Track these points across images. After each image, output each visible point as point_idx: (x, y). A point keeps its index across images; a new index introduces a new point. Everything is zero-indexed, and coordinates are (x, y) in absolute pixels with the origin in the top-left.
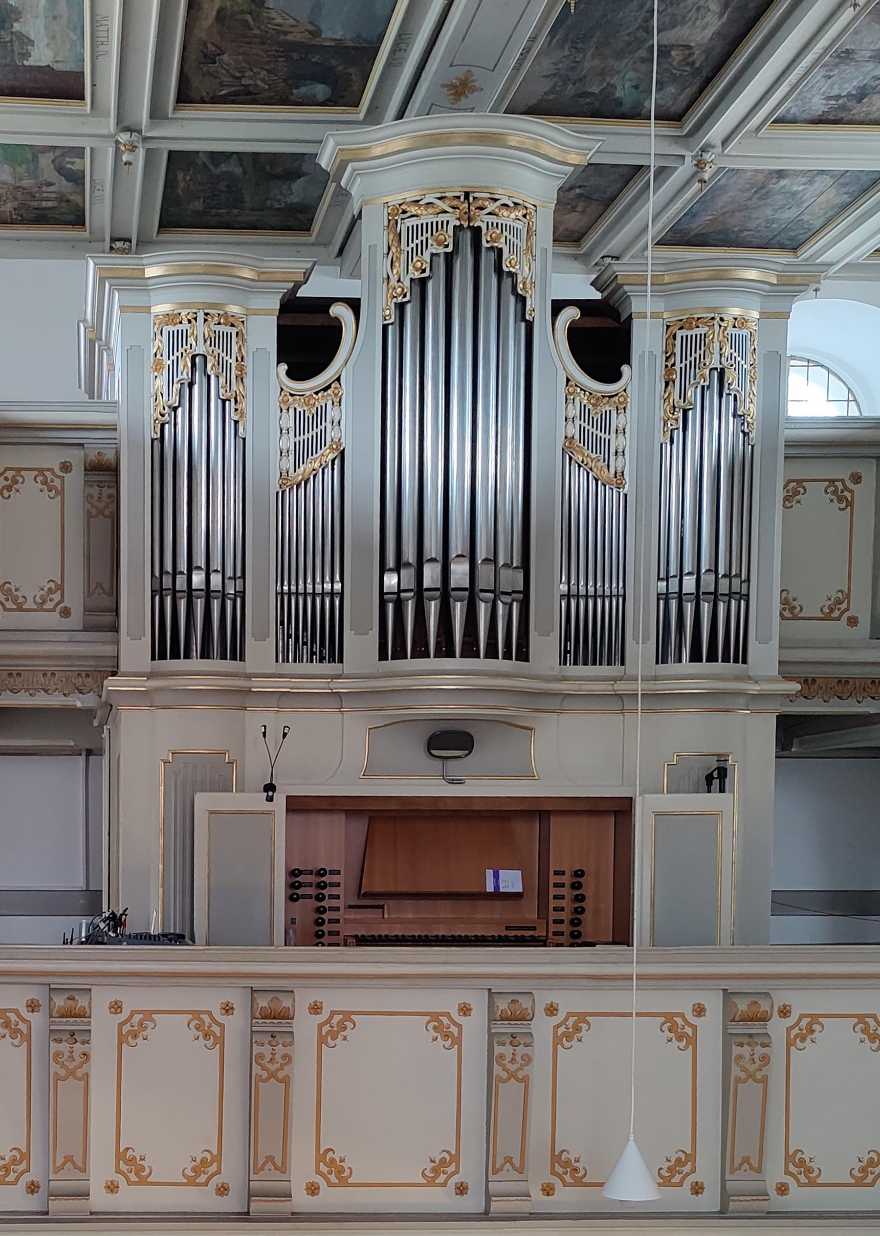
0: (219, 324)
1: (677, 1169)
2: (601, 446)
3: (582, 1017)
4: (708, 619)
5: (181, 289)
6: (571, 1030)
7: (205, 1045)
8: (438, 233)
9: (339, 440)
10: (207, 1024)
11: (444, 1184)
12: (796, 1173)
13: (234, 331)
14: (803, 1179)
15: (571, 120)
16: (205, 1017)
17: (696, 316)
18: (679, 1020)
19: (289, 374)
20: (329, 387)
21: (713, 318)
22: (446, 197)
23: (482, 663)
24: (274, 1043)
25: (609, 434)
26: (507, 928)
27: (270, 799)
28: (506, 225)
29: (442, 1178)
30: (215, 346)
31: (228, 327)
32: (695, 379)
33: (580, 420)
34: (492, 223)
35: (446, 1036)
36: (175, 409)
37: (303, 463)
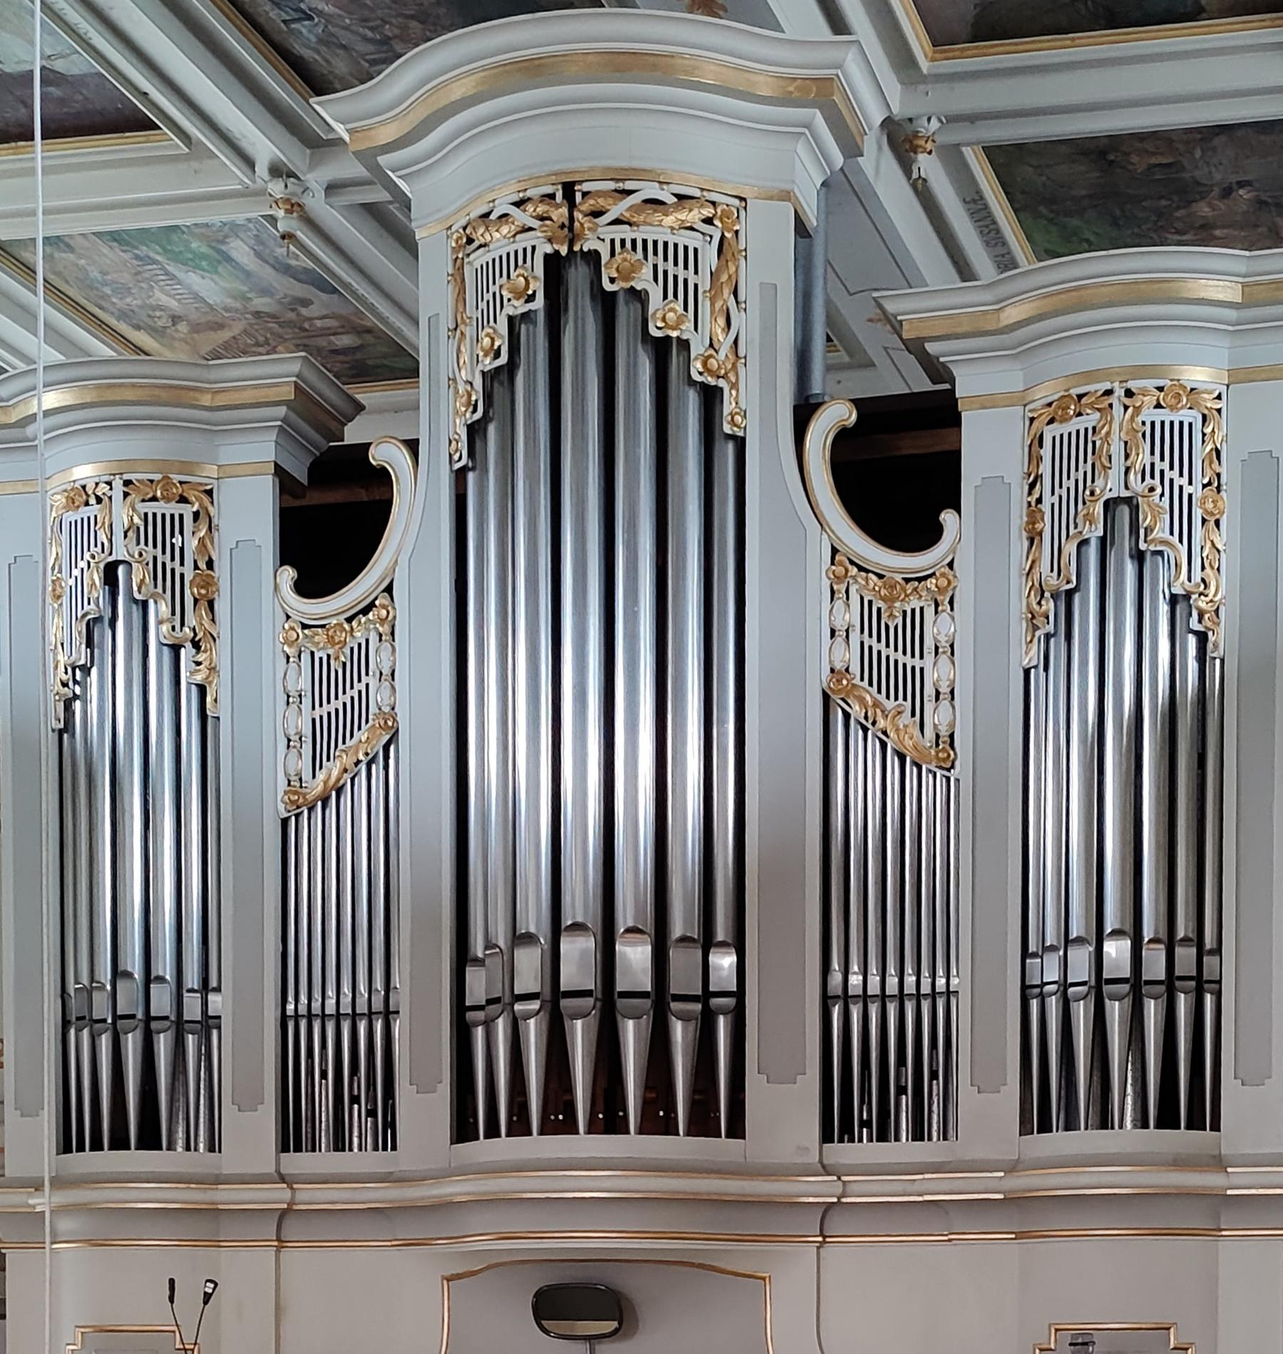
0: (154, 499)
4: (134, 1073)
5: (74, 441)
8: (517, 272)
9: (393, 709)
13: (188, 511)
15: (1073, 39)
17: (1075, 392)
19: (306, 588)
20: (371, 606)
21: (1109, 393)
22: (529, 199)
25: (922, 657)
30: (146, 544)
32: (1076, 527)
36: (86, 670)
37: (328, 760)
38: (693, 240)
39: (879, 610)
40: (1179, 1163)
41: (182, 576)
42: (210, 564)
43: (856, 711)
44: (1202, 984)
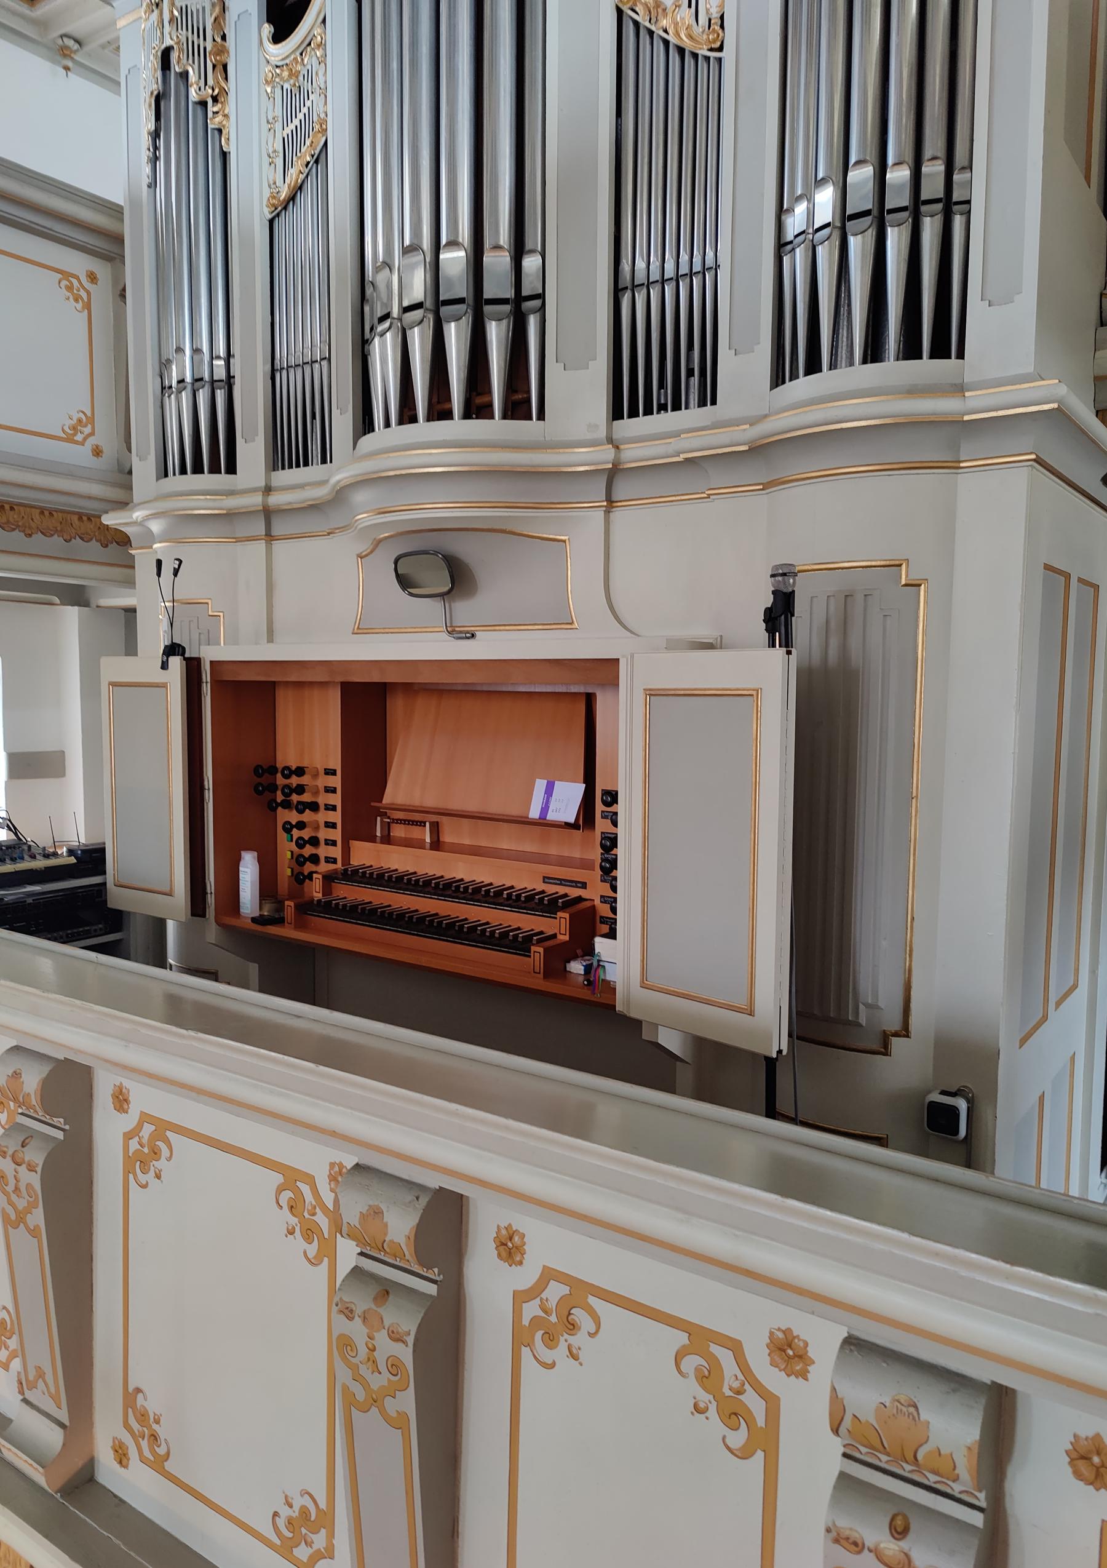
23: (457, 427)
27: (164, 666)
40: (913, 391)
41: (205, 49)
42: (224, 38)
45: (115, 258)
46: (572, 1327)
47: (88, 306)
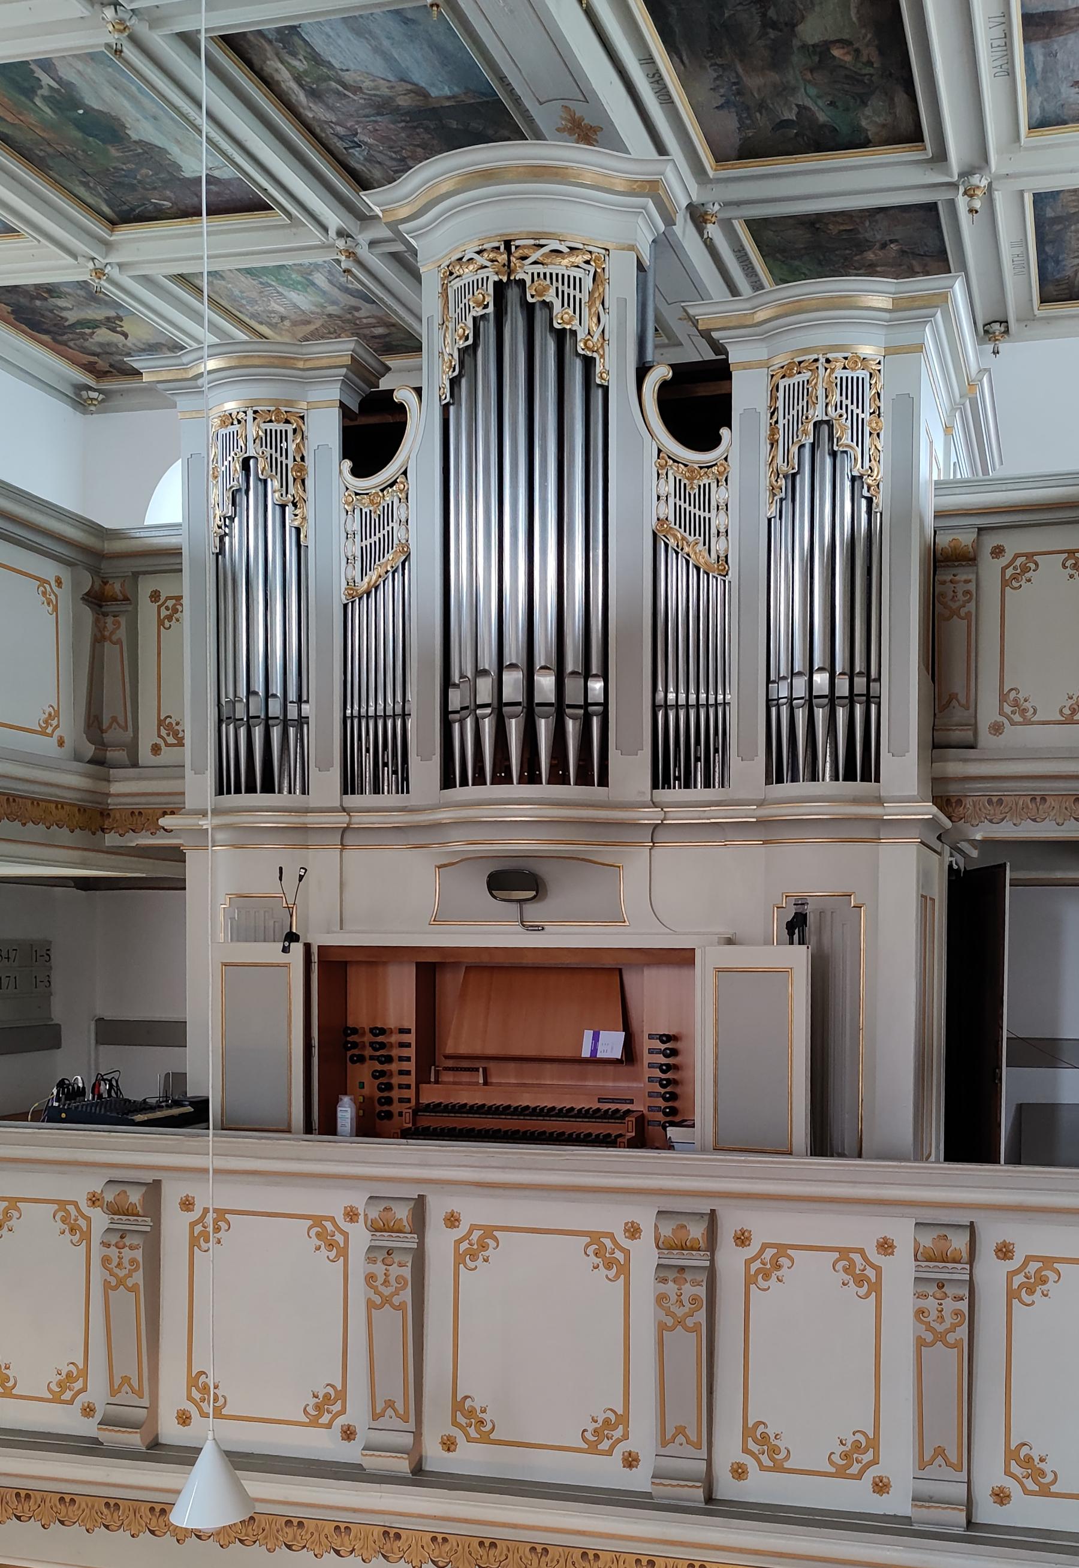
1: (606, 1432)
2: (702, 528)
3: (489, 1232)
6: (475, 1247)
7: (71, 1241)
10: (73, 1217)
11: (329, 1426)
12: (757, 1453)
13: (290, 428)
14: (765, 1460)
15: (796, 158)
16: (71, 1208)
17: (797, 360)
18: (607, 1242)
19: (357, 472)
20: (395, 482)
21: (816, 360)
22: (485, 250)
23: (544, 790)
24: (121, 1244)
25: (709, 512)
26: (600, 1100)
27: (285, 950)
28: (569, 276)
29: (325, 1419)
30: (266, 447)
31: (282, 424)
32: (797, 437)
33: (675, 497)
34: (539, 274)
35: (331, 1246)
36: (232, 519)
38: (578, 273)
39: (685, 484)
42: (303, 459)
43: (672, 542)
44: (869, 699)
45: (77, 565)
46: (779, 1267)
47: (56, 609)
